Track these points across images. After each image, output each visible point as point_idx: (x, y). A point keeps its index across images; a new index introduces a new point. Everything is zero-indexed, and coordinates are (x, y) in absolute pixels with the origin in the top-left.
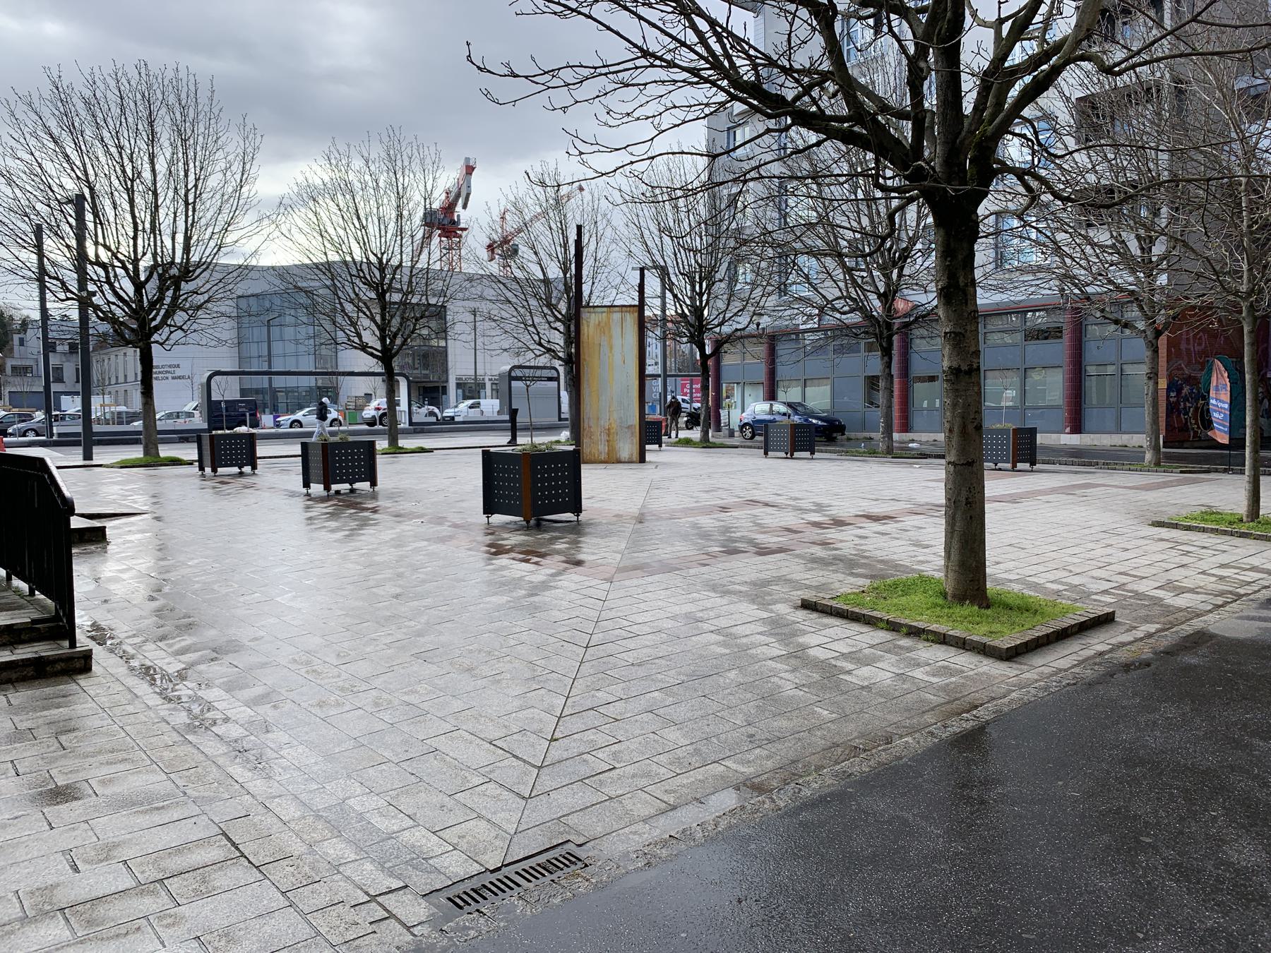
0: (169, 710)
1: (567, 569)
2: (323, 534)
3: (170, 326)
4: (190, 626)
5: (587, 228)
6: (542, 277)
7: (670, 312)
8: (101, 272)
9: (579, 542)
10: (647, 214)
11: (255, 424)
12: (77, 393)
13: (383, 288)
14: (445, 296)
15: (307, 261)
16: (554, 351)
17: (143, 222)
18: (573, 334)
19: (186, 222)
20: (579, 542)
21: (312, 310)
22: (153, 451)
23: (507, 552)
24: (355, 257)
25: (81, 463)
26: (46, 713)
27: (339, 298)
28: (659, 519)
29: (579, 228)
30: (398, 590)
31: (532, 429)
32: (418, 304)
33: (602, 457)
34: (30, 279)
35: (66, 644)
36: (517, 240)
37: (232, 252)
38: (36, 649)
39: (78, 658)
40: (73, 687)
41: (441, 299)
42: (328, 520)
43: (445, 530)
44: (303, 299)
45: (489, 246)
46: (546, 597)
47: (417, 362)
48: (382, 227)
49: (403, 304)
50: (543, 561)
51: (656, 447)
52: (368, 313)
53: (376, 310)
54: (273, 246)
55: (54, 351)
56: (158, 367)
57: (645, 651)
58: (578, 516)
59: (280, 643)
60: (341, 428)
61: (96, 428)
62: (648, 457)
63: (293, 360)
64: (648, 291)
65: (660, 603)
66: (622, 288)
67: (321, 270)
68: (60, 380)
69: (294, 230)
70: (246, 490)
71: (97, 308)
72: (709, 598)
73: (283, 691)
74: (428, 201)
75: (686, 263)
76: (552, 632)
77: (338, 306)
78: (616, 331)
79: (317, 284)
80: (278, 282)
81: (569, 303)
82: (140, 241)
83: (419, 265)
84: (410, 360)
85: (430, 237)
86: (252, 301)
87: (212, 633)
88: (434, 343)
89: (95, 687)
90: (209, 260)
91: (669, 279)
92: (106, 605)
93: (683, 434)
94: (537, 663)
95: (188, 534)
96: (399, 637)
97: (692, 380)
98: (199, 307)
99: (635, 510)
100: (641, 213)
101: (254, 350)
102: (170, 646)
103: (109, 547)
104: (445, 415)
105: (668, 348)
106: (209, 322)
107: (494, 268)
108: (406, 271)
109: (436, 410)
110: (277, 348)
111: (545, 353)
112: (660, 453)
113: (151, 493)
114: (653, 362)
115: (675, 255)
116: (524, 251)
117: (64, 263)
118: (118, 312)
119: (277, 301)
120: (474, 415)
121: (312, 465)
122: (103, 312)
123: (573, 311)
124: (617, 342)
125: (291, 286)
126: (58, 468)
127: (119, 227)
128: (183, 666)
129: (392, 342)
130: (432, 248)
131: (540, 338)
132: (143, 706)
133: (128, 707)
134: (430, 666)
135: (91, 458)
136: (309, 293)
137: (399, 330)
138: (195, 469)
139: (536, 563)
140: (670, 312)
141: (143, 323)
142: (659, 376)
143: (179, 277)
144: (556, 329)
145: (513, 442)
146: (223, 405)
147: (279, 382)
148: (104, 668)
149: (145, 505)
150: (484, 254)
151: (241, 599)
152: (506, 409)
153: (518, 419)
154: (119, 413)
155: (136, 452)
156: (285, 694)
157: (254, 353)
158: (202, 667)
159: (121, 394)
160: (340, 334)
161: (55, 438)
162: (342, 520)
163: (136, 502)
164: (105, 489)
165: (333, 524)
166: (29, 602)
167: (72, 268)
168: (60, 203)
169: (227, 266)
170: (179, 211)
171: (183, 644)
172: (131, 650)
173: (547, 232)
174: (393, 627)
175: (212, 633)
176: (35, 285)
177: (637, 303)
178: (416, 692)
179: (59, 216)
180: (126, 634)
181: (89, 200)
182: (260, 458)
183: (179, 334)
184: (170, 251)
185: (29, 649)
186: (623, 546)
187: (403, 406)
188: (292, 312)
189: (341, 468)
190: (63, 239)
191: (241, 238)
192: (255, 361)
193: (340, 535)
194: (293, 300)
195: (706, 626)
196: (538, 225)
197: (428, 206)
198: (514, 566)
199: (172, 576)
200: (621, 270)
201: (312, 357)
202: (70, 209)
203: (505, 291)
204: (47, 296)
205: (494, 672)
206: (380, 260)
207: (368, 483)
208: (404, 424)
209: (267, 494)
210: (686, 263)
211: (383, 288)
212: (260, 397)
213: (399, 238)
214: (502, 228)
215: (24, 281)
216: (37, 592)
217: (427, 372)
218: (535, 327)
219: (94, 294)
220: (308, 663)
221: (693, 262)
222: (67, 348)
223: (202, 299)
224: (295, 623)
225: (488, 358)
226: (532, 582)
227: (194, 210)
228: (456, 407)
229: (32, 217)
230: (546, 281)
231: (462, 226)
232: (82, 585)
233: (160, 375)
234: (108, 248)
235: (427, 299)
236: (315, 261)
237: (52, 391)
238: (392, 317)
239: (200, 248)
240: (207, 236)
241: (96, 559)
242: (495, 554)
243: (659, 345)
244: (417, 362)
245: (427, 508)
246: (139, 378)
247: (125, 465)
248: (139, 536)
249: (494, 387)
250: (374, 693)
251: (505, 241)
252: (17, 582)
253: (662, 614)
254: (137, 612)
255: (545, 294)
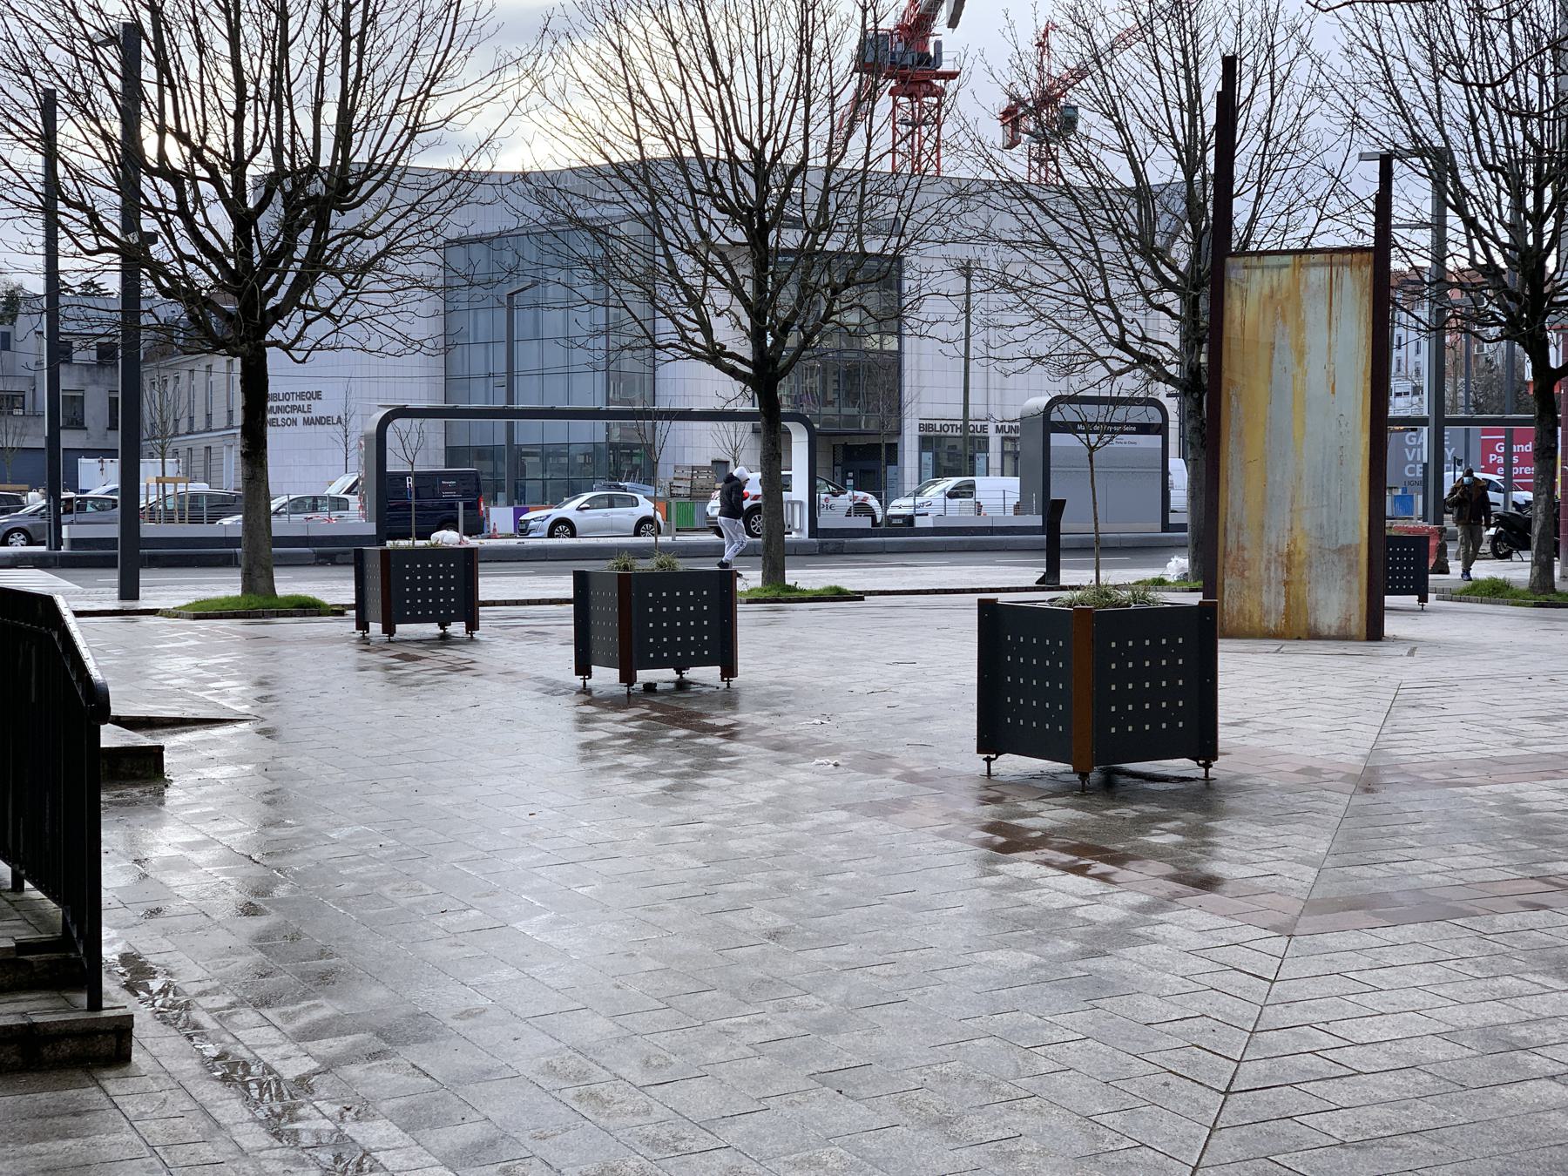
0: (284, 1160)
1: (1178, 895)
2: (618, 782)
3: (305, 307)
4: (325, 979)
5: (1249, 61)
6: (1131, 183)
7: (1457, 261)
8: (169, 191)
9: (1210, 832)
10: (1402, 23)
11: (476, 527)
12: (110, 453)
13: (761, 219)
14: (902, 234)
15: (599, 161)
16: (1155, 362)
17: (257, 82)
18: (1204, 321)
19: (344, 77)
20: (1210, 832)
21: (605, 270)
22: (261, 583)
23: (1033, 845)
24: (704, 150)
25: (115, 605)
26: (38, 1147)
27: (665, 243)
28: (1418, 783)
29: (1230, 64)
30: (781, 922)
31: (1099, 549)
32: (840, 254)
33: (1272, 622)
34: (29, 207)
35: (82, 999)
36: (1073, 97)
37: (438, 142)
38: (23, 1007)
39: (105, 1033)
40: (91, 1095)
41: (894, 241)
42: (627, 750)
43: (887, 786)
44: (585, 246)
45: (1006, 114)
46: (1127, 960)
47: (831, 386)
48: (766, 79)
49: (806, 254)
50: (1121, 874)
51: (1412, 600)
52: (726, 276)
53: (745, 270)
54: (525, 126)
55: (69, 361)
56: (276, 397)
57: (1375, 1112)
58: (1207, 766)
59: (522, 1026)
60: (661, 539)
61: (148, 530)
62: (1391, 626)
63: (561, 381)
64: (1400, 211)
65: (1417, 997)
66: (1334, 205)
67: (627, 180)
68: (78, 424)
69: (573, 89)
70: (454, 677)
71: (158, 269)
72: (1546, 990)
73: (525, 1138)
74: (870, 14)
75: (1500, 141)
76: (1139, 1048)
77: (663, 261)
78: (1315, 312)
79: (615, 211)
80: (534, 211)
81: (1197, 245)
82: (248, 122)
83: (845, 164)
84: (815, 382)
85: (873, 97)
86: (478, 251)
87: (377, 995)
88: (872, 343)
89: (138, 1099)
90: (389, 161)
91: (1456, 181)
92: (157, 921)
93: (1483, 570)
94: (1104, 1120)
95: (331, 770)
96: (783, 1029)
97: (1510, 434)
98: (365, 268)
99: (1352, 759)
100: (1386, 22)
101: (477, 360)
102: (289, 1018)
103: (168, 792)
104: (891, 512)
105: (1449, 353)
106: (386, 299)
107: (1017, 164)
108: (815, 179)
109: (873, 502)
110: (527, 355)
111: (1132, 366)
112: (1422, 618)
113: (256, 676)
114: (1406, 386)
115: (1473, 120)
116: (1091, 122)
117: (96, 174)
118: (202, 279)
119: (530, 251)
120: (960, 511)
121: (596, 623)
122: (170, 278)
123: (1206, 265)
124: (1316, 338)
125: (561, 218)
126: (78, 614)
127: (209, 91)
128: (315, 1065)
129: (779, 342)
130: (877, 123)
131: (1123, 331)
132: (232, 1147)
133: (202, 1148)
134: (851, 1104)
135: (135, 596)
136: (599, 232)
137: (795, 315)
138: (348, 626)
139: (1103, 877)
140: (1457, 261)
141: (251, 301)
142: (1423, 422)
143: (326, 200)
144: (1162, 308)
145: (1050, 580)
146: (410, 482)
147: (530, 433)
148: (155, 1058)
149: (244, 702)
150: (994, 133)
151: (441, 921)
152: (1035, 500)
153: (1065, 525)
154: (195, 497)
155: (226, 585)
156: (530, 1144)
157: (478, 368)
158: (355, 1071)
159: (199, 454)
160: (665, 325)
161: (64, 549)
162: (658, 752)
163: (224, 695)
164: (163, 664)
165: (639, 761)
166: (11, 903)
167: (112, 183)
168: (93, 45)
169: (427, 173)
170: (331, 53)
171: (317, 1015)
172: (205, 1020)
173: (1148, 76)
174: (770, 1007)
175: (377, 995)
176: (38, 222)
177: (1369, 242)
178: (820, 1164)
179: (89, 71)
180: (199, 987)
181: (151, 35)
182: (486, 604)
183: (324, 325)
184: (310, 143)
185: (11, 1007)
186: (1321, 847)
187: (799, 490)
188: (563, 275)
189: (658, 633)
190: (97, 122)
191: (458, 112)
192: (478, 387)
193: (653, 786)
194: (564, 249)
195: (1535, 1062)
196: (1126, 58)
197: (870, 25)
198: (1050, 881)
199: (297, 862)
200: (1333, 160)
201: (600, 377)
202: (111, 56)
203: (1043, 220)
204: (61, 245)
205: (999, 1134)
206: (758, 156)
207: (717, 670)
208: (798, 532)
209: (498, 687)
210: (1500, 141)
211: (761, 219)
212: (487, 466)
213: (801, 102)
214: (1040, 68)
215: (19, 212)
216: (27, 885)
217: (855, 411)
218: (1111, 304)
219: (152, 238)
220: (581, 1076)
221: (1519, 137)
222: (93, 355)
223: (370, 248)
224: (555, 982)
225: (996, 378)
226: (1091, 923)
227: (361, 53)
228: (918, 493)
229: (39, 75)
230: (1143, 193)
231: (946, 67)
232: (114, 877)
233: (280, 416)
234: (183, 138)
235: (860, 243)
236: (615, 159)
237: (63, 446)
238: (780, 285)
239: (372, 136)
240: (387, 109)
241: (142, 818)
242: (1005, 849)
243: (1425, 345)
244: (831, 386)
245: (848, 733)
246: (238, 419)
247: (204, 612)
248: (228, 770)
249: (1009, 447)
250: (724, 1158)
251: (1047, 99)
252: (32, 892)
253: (1420, 1025)
254: (222, 939)
255: (1139, 225)
